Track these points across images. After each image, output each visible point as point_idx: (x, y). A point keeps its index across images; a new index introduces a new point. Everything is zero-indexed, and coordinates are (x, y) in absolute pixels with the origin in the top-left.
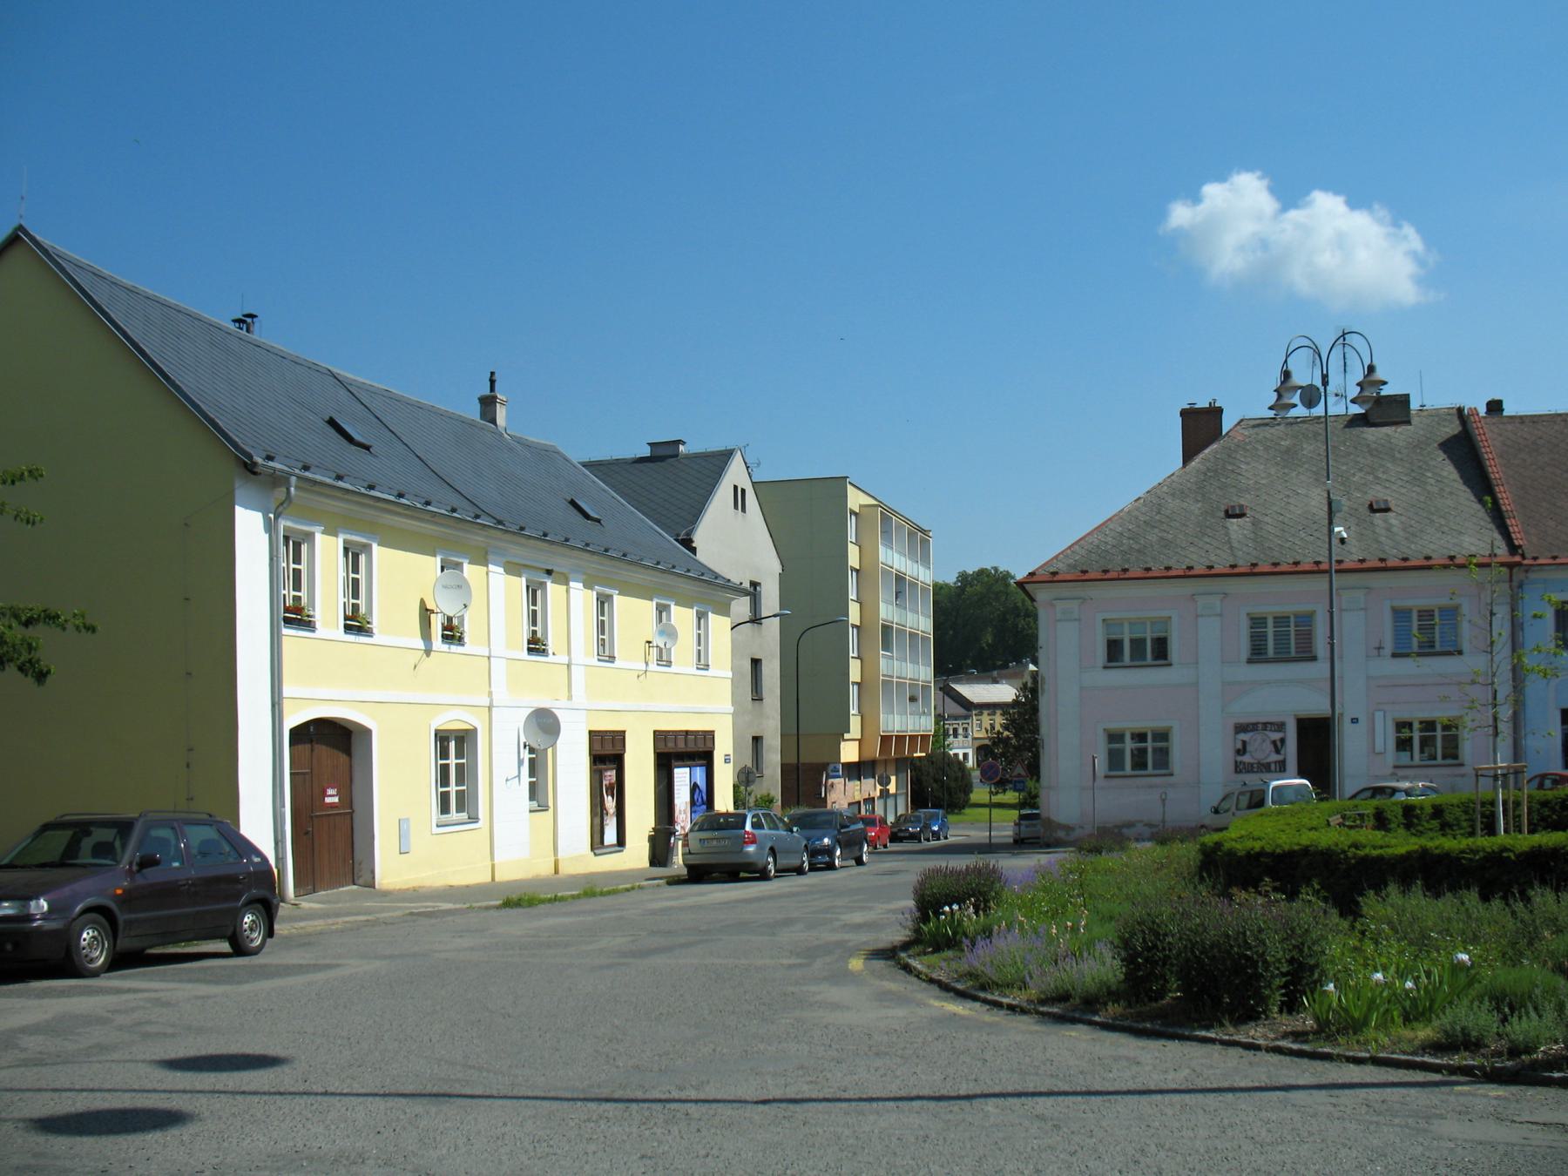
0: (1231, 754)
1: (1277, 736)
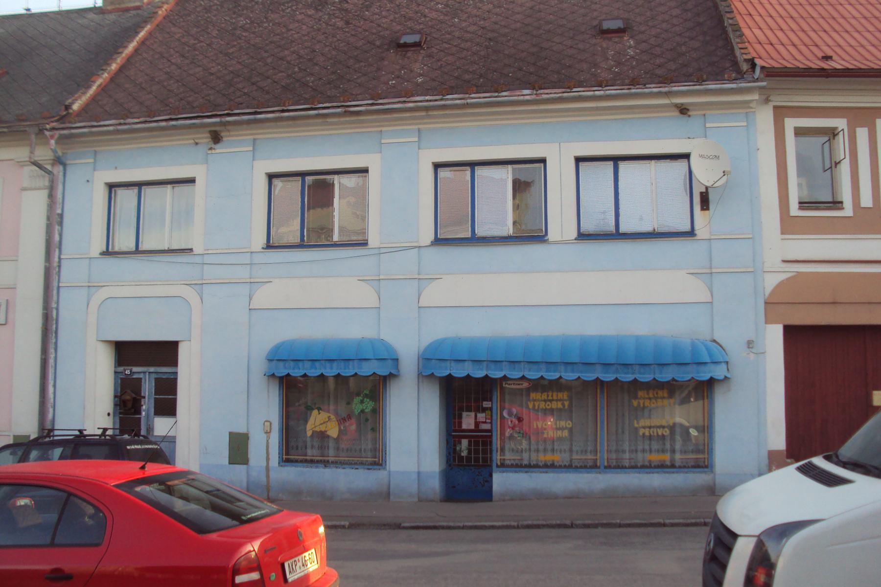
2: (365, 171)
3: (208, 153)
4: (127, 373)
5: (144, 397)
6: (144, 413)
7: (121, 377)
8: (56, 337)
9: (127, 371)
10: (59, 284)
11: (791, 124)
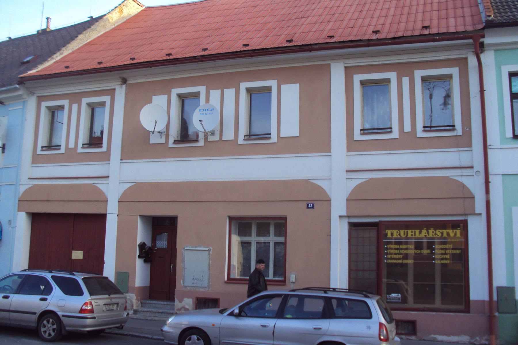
11: (357, 78)
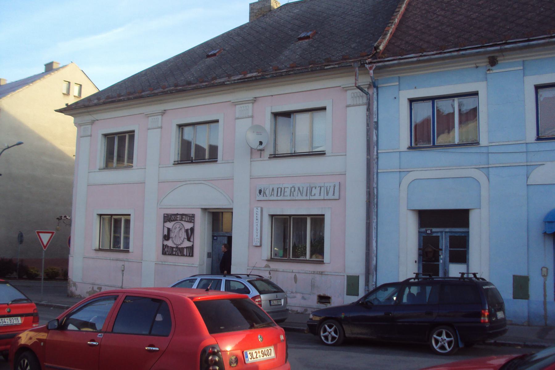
0: (161, 237)
1: (188, 226)
2: (476, 94)
3: (487, 73)
4: (428, 232)
5: (441, 250)
6: (441, 261)
7: (424, 235)
8: (377, 208)
9: (428, 231)
10: (377, 171)
